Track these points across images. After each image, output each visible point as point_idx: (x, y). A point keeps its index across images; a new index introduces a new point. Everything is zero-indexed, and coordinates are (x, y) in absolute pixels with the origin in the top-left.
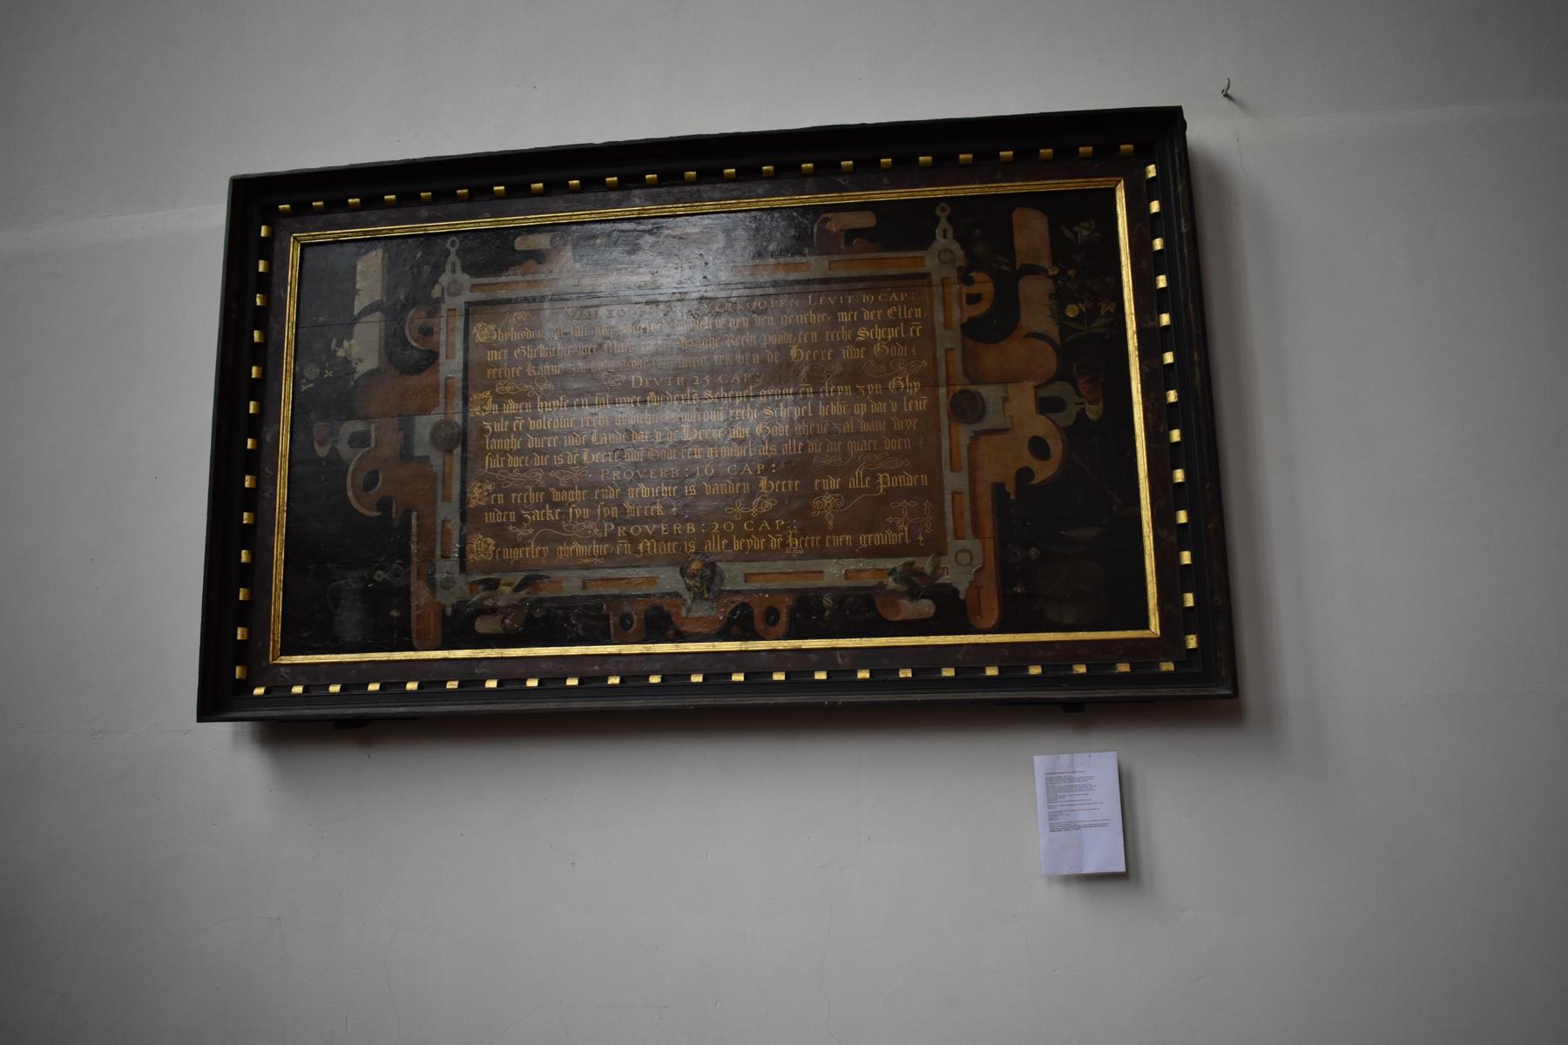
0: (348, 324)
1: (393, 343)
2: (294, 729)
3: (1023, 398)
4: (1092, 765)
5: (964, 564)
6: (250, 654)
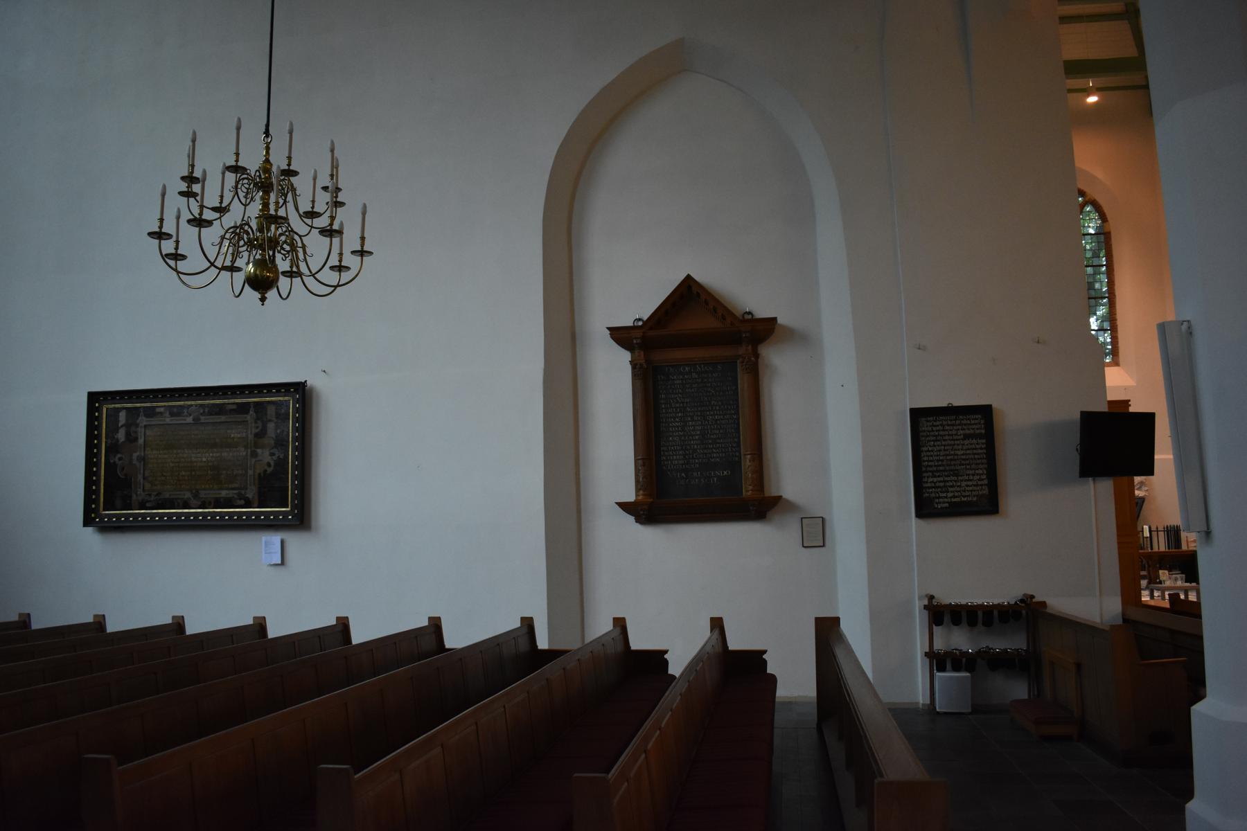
0: (117, 430)
1: (128, 434)
3: (267, 453)
4: (275, 538)
5: (251, 493)
6: (96, 511)
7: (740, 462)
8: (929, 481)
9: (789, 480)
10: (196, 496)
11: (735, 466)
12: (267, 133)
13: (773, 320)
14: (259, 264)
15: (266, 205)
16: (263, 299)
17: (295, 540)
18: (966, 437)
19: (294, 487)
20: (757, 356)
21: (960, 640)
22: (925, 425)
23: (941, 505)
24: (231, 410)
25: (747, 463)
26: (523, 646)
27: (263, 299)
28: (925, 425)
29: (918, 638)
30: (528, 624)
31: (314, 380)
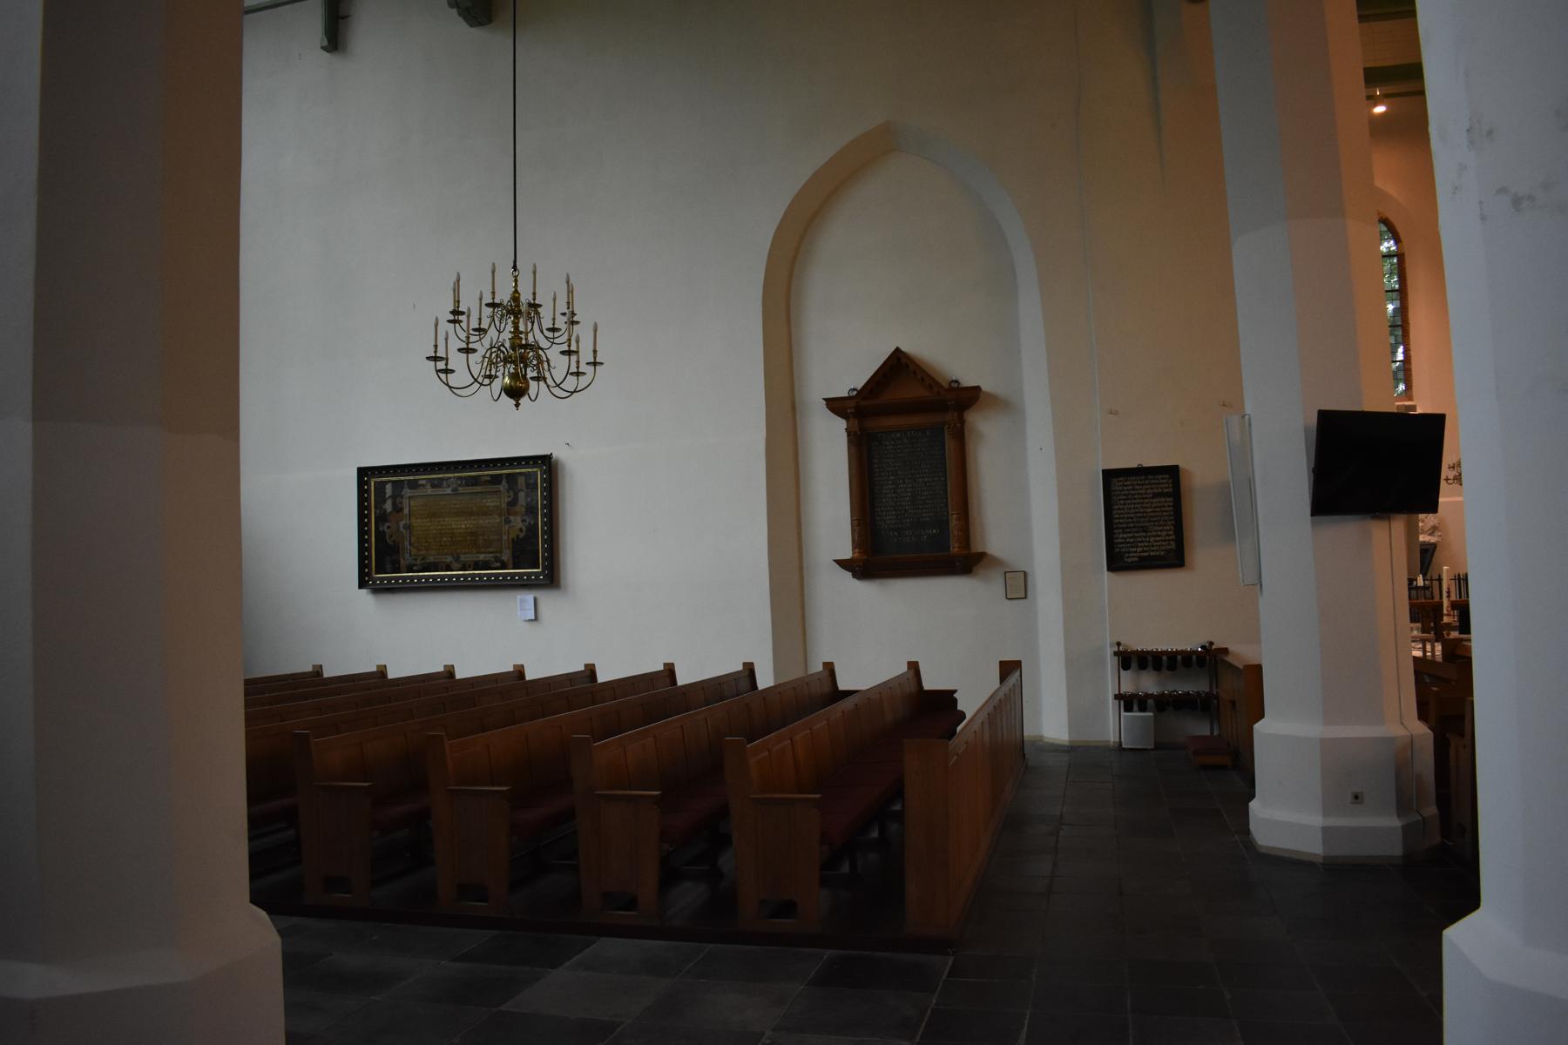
0: (384, 501)
1: (394, 505)
2: (377, 590)
3: (519, 519)
4: (528, 597)
5: (506, 556)
6: (369, 574)
7: (947, 522)
8: (1120, 537)
9: (994, 536)
10: (457, 559)
11: (943, 524)
12: (515, 268)
13: (977, 389)
14: (514, 376)
15: (516, 327)
16: (517, 405)
17: (547, 599)
18: (1155, 495)
19: (544, 550)
20: (962, 421)
21: (1149, 684)
22: (1117, 484)
23: (1132, 558)
24: (487, 482)
25: (954, 522)
26: (827, 688)
27: (517, 405)
28: (1117, 484)
29: (1112, 681)
30: (749, 669)
31: (559, 453)
